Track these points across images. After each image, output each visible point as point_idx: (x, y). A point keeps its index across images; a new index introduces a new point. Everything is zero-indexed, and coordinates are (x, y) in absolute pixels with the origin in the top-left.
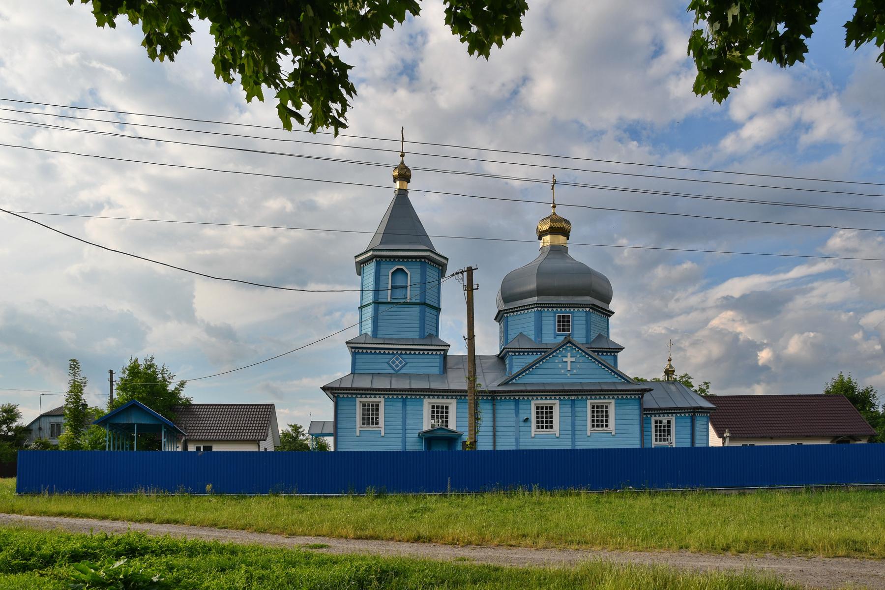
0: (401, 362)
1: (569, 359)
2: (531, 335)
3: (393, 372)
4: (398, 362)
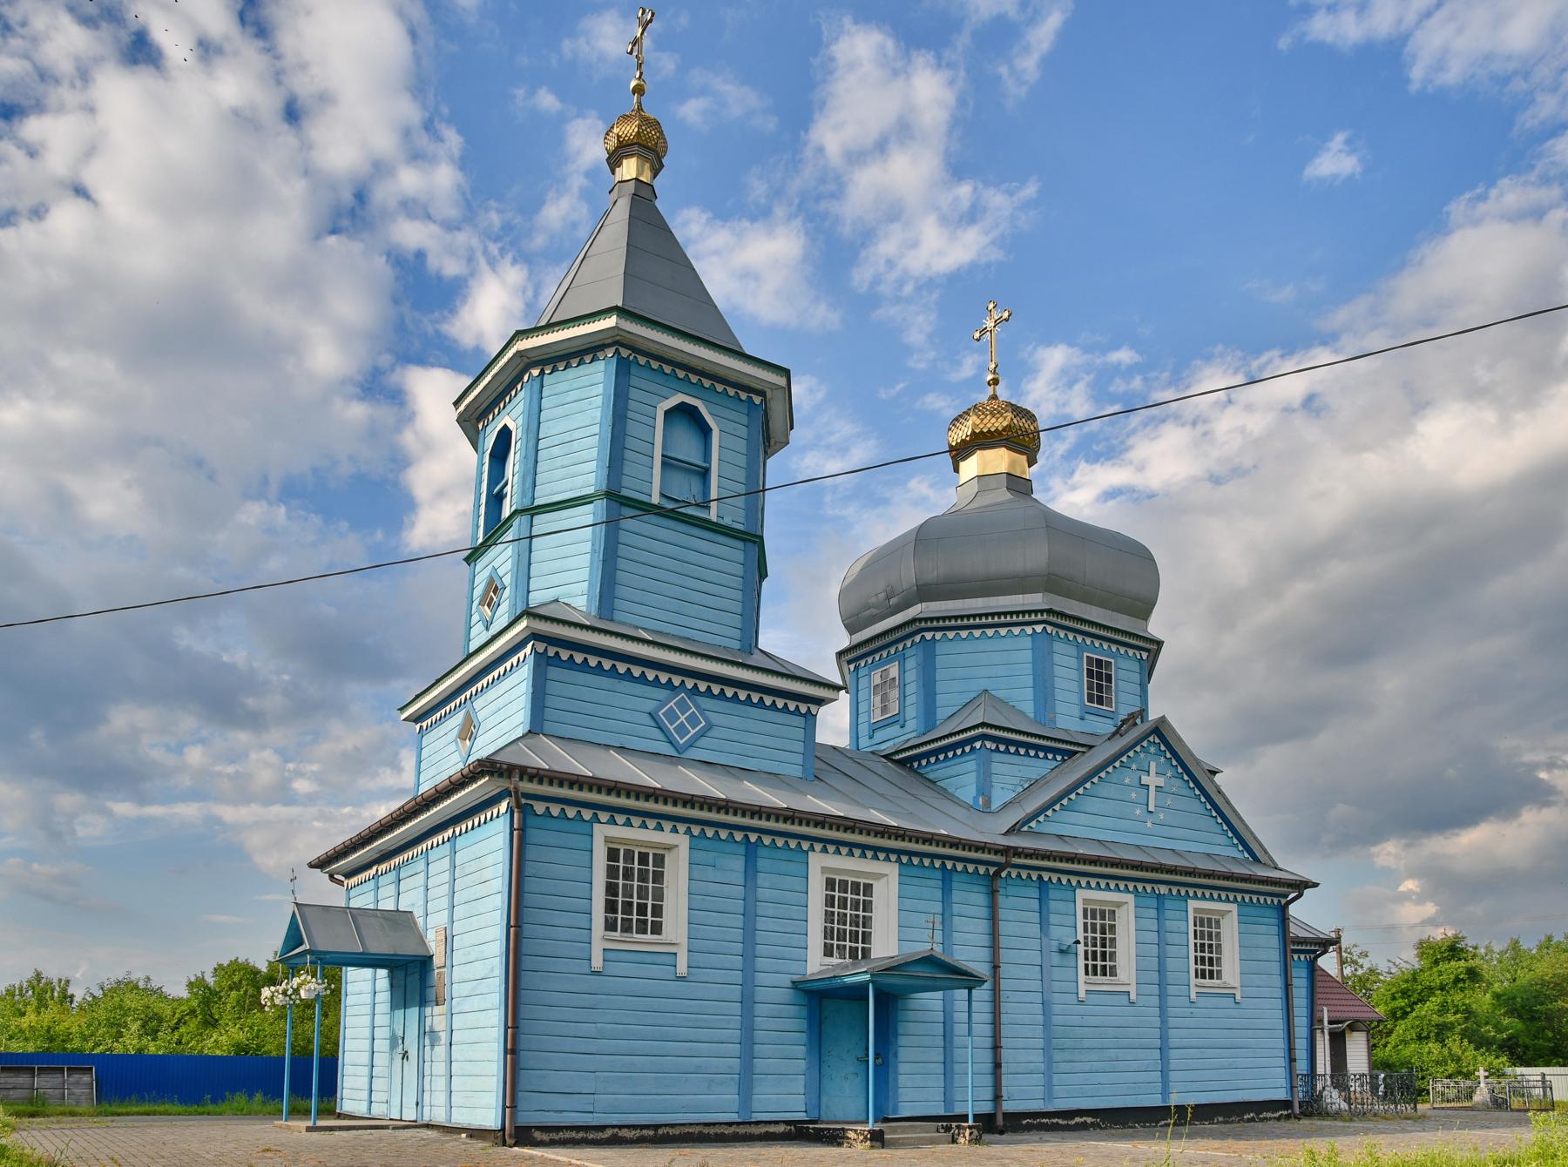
0: (693, 720)
1: (1152, 780)
2: (1025, 700)
3: (666, 749)
4: (682, 714)
